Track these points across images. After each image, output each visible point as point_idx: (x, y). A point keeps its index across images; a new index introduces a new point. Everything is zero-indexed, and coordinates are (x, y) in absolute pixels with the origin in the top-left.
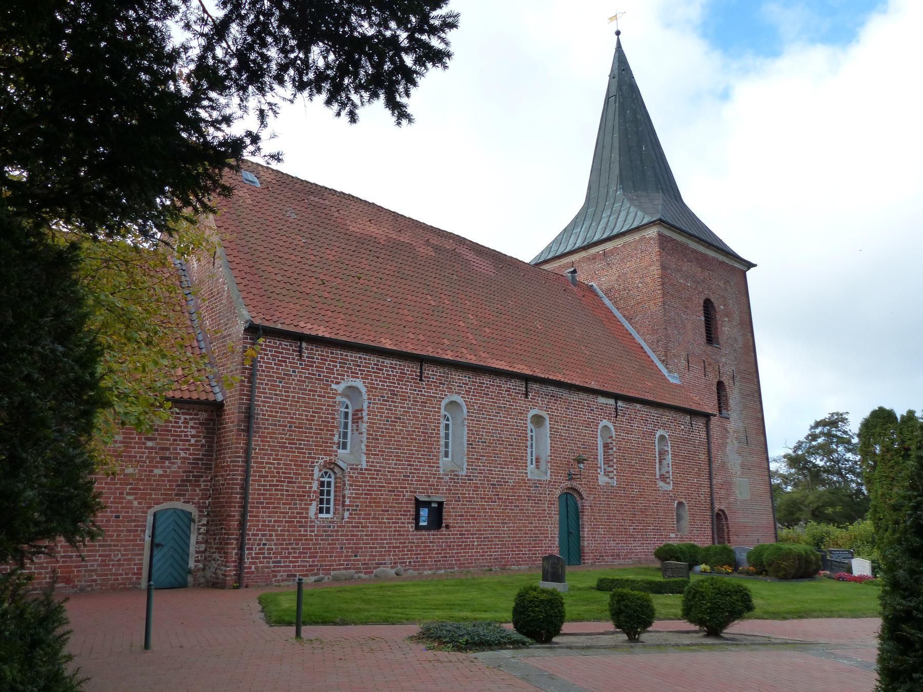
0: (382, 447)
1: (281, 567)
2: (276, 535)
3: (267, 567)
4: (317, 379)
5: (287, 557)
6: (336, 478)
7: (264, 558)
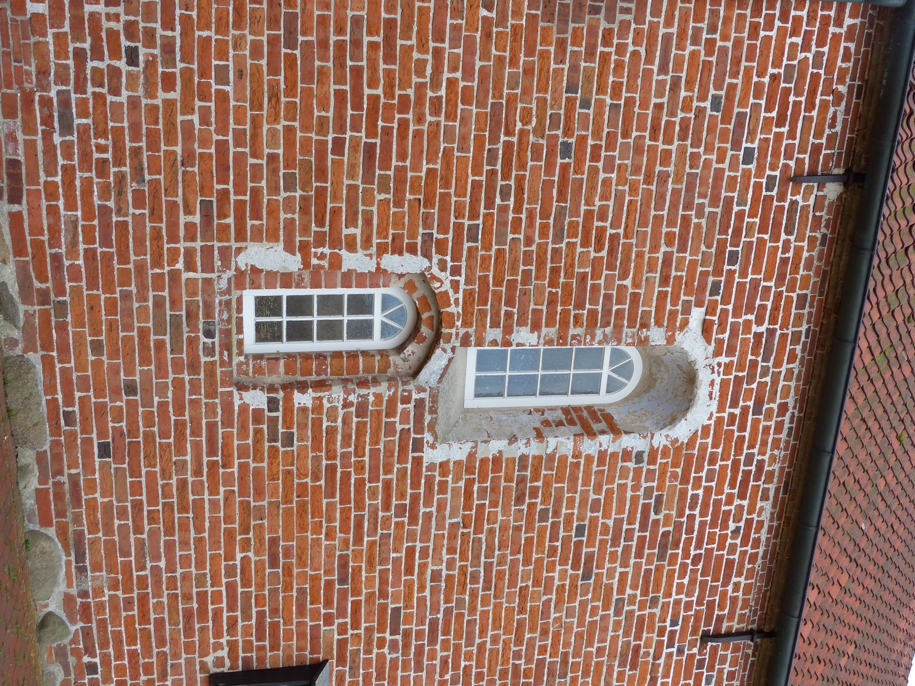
0: (492, 519)
1: (47, 136)
2: (169, 104)
3: (43, 72)
4: (722, 245)
5: (85, 157)
6: (383, 353)
7: (80, 55)
